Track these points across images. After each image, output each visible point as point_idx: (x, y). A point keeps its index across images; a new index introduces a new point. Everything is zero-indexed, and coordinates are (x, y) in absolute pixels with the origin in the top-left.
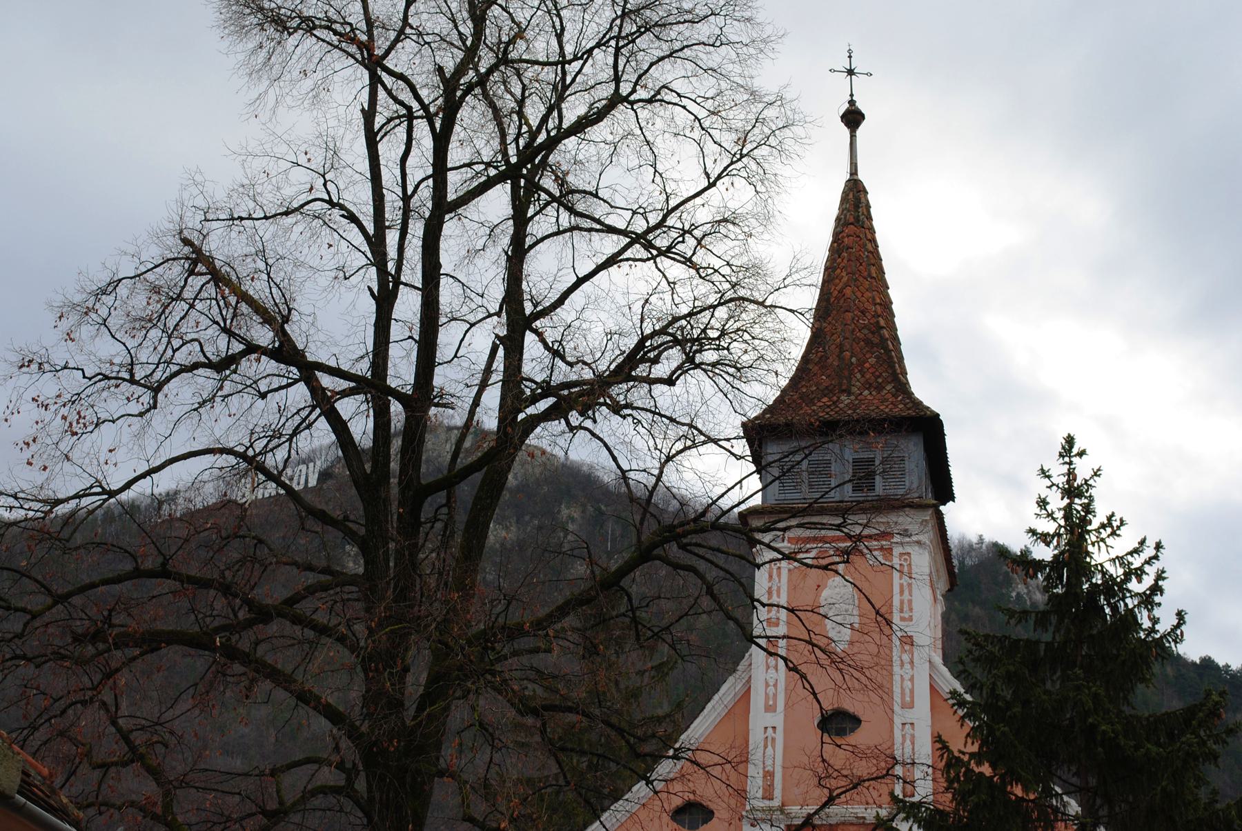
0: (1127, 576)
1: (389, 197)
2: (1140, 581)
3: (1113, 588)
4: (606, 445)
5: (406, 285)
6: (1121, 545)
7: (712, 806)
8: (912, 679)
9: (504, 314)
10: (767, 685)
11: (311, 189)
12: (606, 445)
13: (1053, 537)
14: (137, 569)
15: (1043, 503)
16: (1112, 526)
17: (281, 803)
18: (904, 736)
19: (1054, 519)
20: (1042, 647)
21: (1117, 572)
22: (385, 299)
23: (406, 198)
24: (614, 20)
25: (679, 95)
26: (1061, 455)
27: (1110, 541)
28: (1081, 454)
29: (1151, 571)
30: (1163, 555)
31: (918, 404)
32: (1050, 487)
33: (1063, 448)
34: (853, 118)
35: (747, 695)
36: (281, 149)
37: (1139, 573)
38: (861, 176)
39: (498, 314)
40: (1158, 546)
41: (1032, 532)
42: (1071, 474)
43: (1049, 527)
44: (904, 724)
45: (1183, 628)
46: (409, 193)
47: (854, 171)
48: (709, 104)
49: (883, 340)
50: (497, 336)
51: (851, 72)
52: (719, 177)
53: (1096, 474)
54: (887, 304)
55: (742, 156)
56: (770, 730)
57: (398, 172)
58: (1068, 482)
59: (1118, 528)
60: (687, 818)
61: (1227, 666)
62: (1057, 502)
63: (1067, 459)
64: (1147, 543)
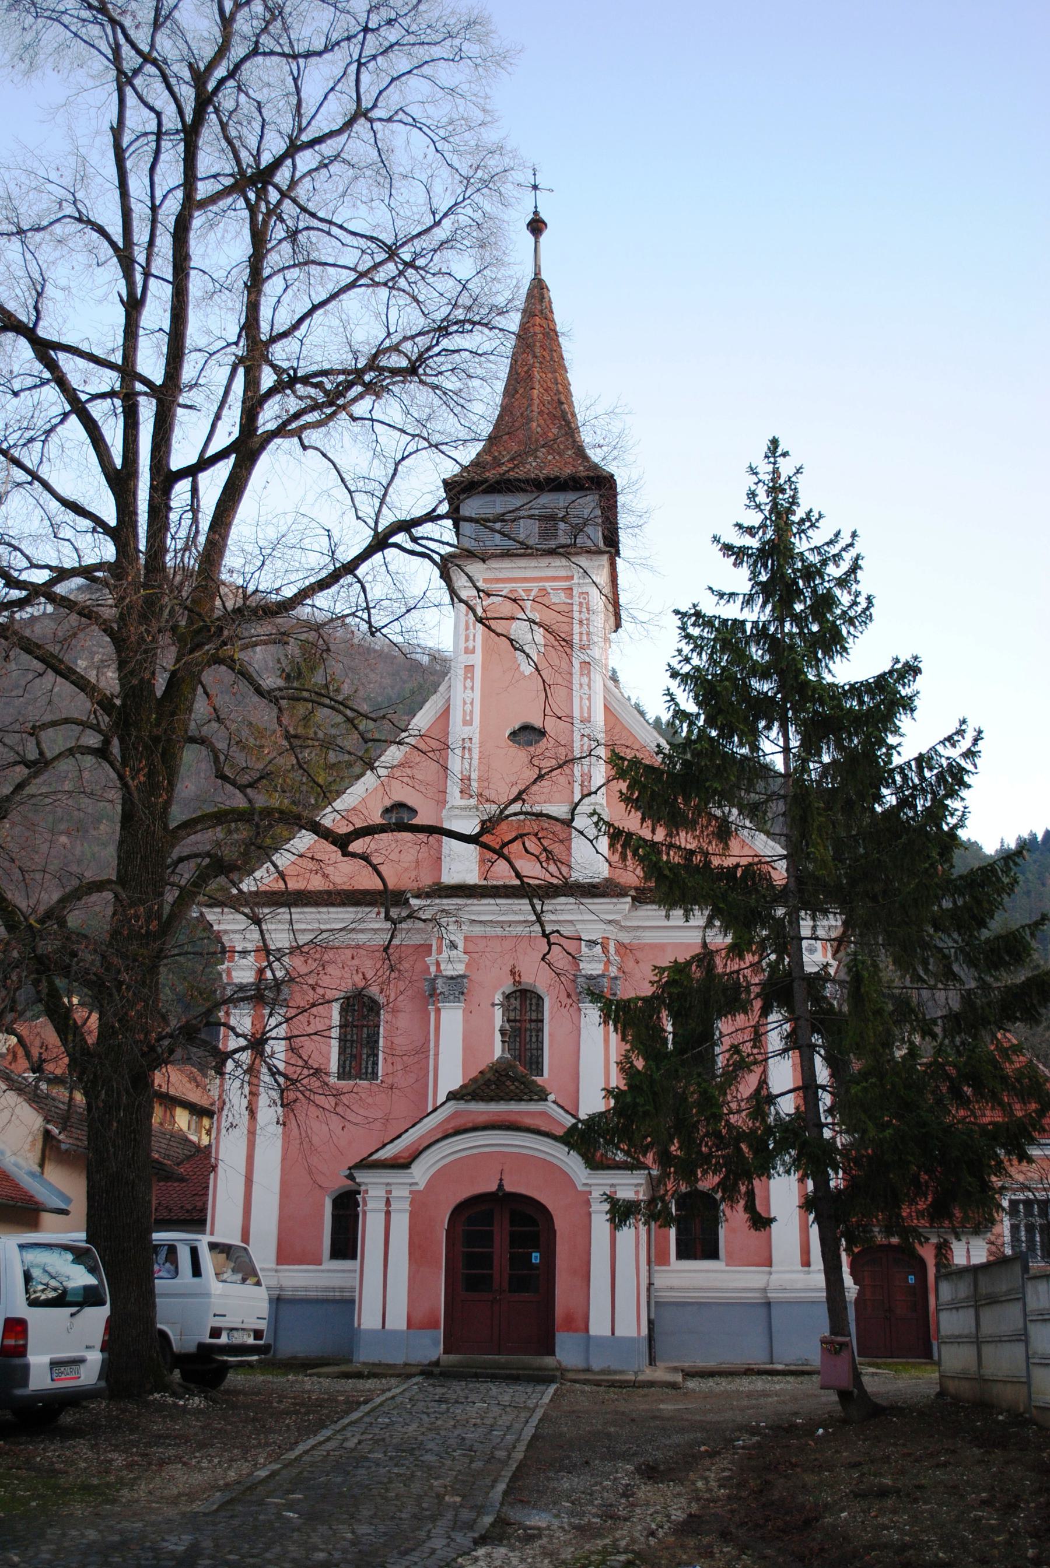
0: (824, 563)
1: (135, 206)
2: (838, 566)
3: (811, 573)
5: (157, 277)
6: (819, 536)
7: (416, 807)
8: (589, 699)
9: (241, 344)
10: (465, 703)
15: (752, 495)
16: (810, 521)
17: (41, 753)
19: (761, 511)
20: (748, 626)
21: (814, 558)
22: (133, 305)
23: (154, 209)
24: (348, 65)
26: (767, 457)
27: (810, 533)
28: (785, 454)
29: (848, 557)
34: (536, 226)
35: (446, 713)
37: (837, 558)
38: (544, 276)
39: (236, 344)
40: (854, 535)
41: (740, 526)
42: (776, 472)
43: (754, 519)
45: (872, 610)
46: (158, 203)
47: (537, 273)
48: (442, 133)
49: (564, 414)
51: (535, 187)
52: (445, 215)
53: (798, 471)
54: (567, 386)
58: (772, 480)
62: (762, 498)
63: (772, 460)
64: (842, 535)
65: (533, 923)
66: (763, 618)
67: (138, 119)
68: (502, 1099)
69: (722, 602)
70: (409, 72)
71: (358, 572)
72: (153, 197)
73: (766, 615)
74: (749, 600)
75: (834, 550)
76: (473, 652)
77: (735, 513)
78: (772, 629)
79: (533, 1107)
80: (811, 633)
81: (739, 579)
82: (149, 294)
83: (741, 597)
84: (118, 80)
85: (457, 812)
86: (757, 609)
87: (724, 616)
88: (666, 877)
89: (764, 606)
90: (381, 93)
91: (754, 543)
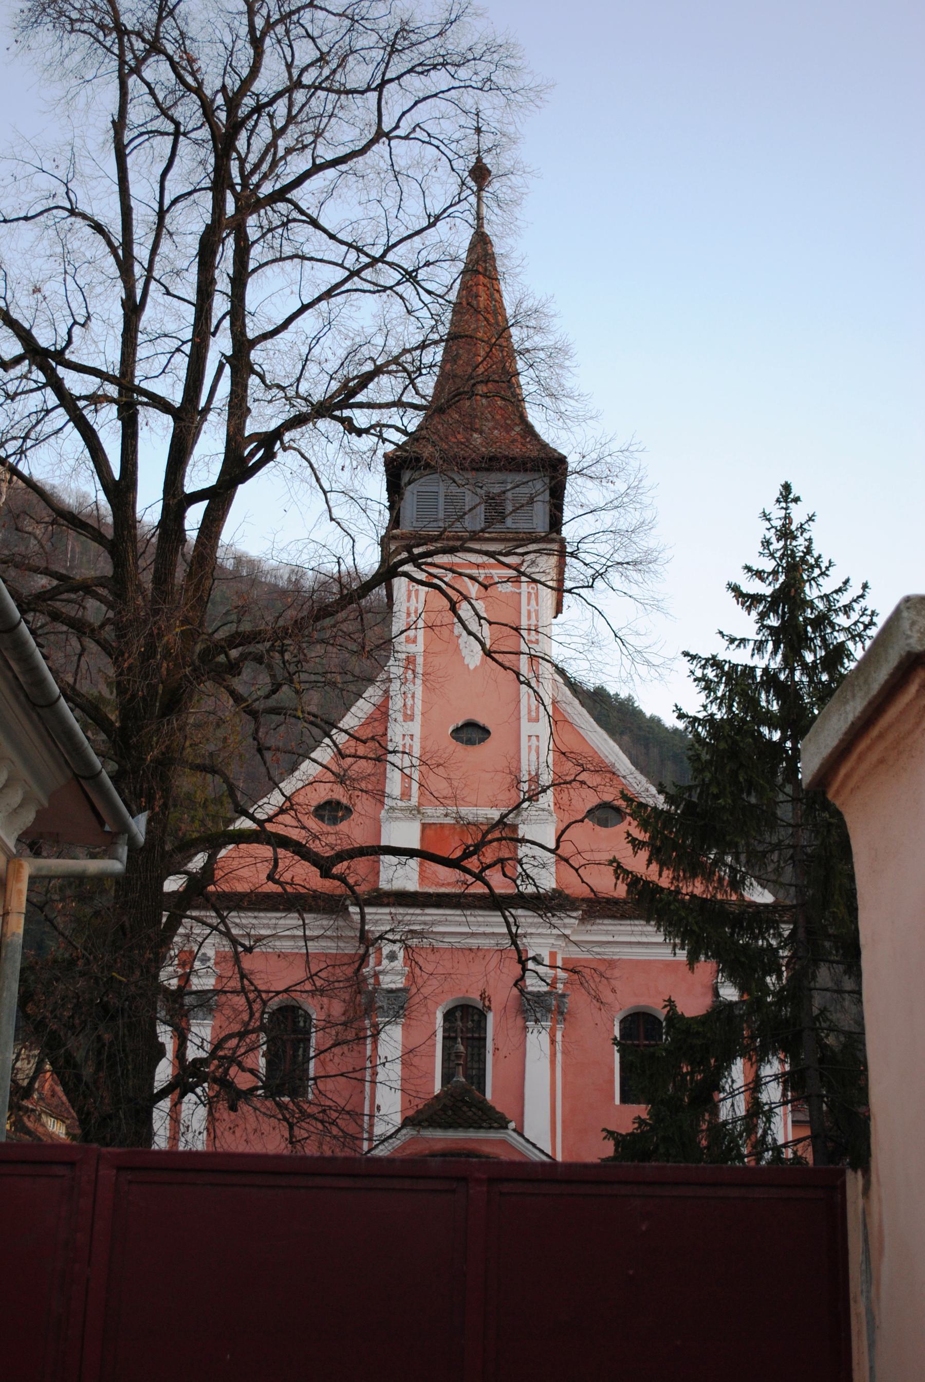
2: (848, 617)
4: (311, 466)
6: (828, 585)
11: (54, 196)
12: (311, 466)
13: (769, 574)
14: (47, 568)
18: (530, 747)
20: (759, 673)
25: (429, 135)
26: (778, 501)
28: (796, 500)
30: (869, 594)
31: (545, 446)
32: (768, 529)
33: (781, 494)
36: (28, 154)
40: (865, 586)
41: (748, 569)
42: (787, 517)
43: (768, 565)
44: (404, 735)
46: (165, 208)
50: (223, 355)
55: (460, 201)
56: (407, 738)
57: (157, 187)
58: (784, 525)
59: (827, 568)
60: (326, 813)
61: (617, 695)
63: (783, 505)
65: (356, 884)
66: (773, 665)
67: (140, 112)
68: (470, 1127)
69: (733, 646)
70: (435, 95)
71: (49, 390)
72: (161, 203)
73: (776, 663)
74: (760, 647)
75: (844, 599)
76: (537, 720)
77: (742, 550)
78: (782, 677)
79: (493, 1135)
80: (820, 682)
81: (747, 624)
82: (149, 299)
83: (752, 643)
84: (120, 70)
85: (398, 814)
86: (767, 656)
87: (734, 661)
88: (693, 931)
89: (775, 652)
90: (404, 114)
91: (766, 590)
